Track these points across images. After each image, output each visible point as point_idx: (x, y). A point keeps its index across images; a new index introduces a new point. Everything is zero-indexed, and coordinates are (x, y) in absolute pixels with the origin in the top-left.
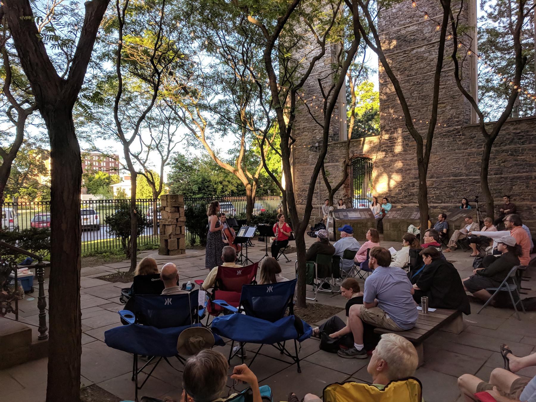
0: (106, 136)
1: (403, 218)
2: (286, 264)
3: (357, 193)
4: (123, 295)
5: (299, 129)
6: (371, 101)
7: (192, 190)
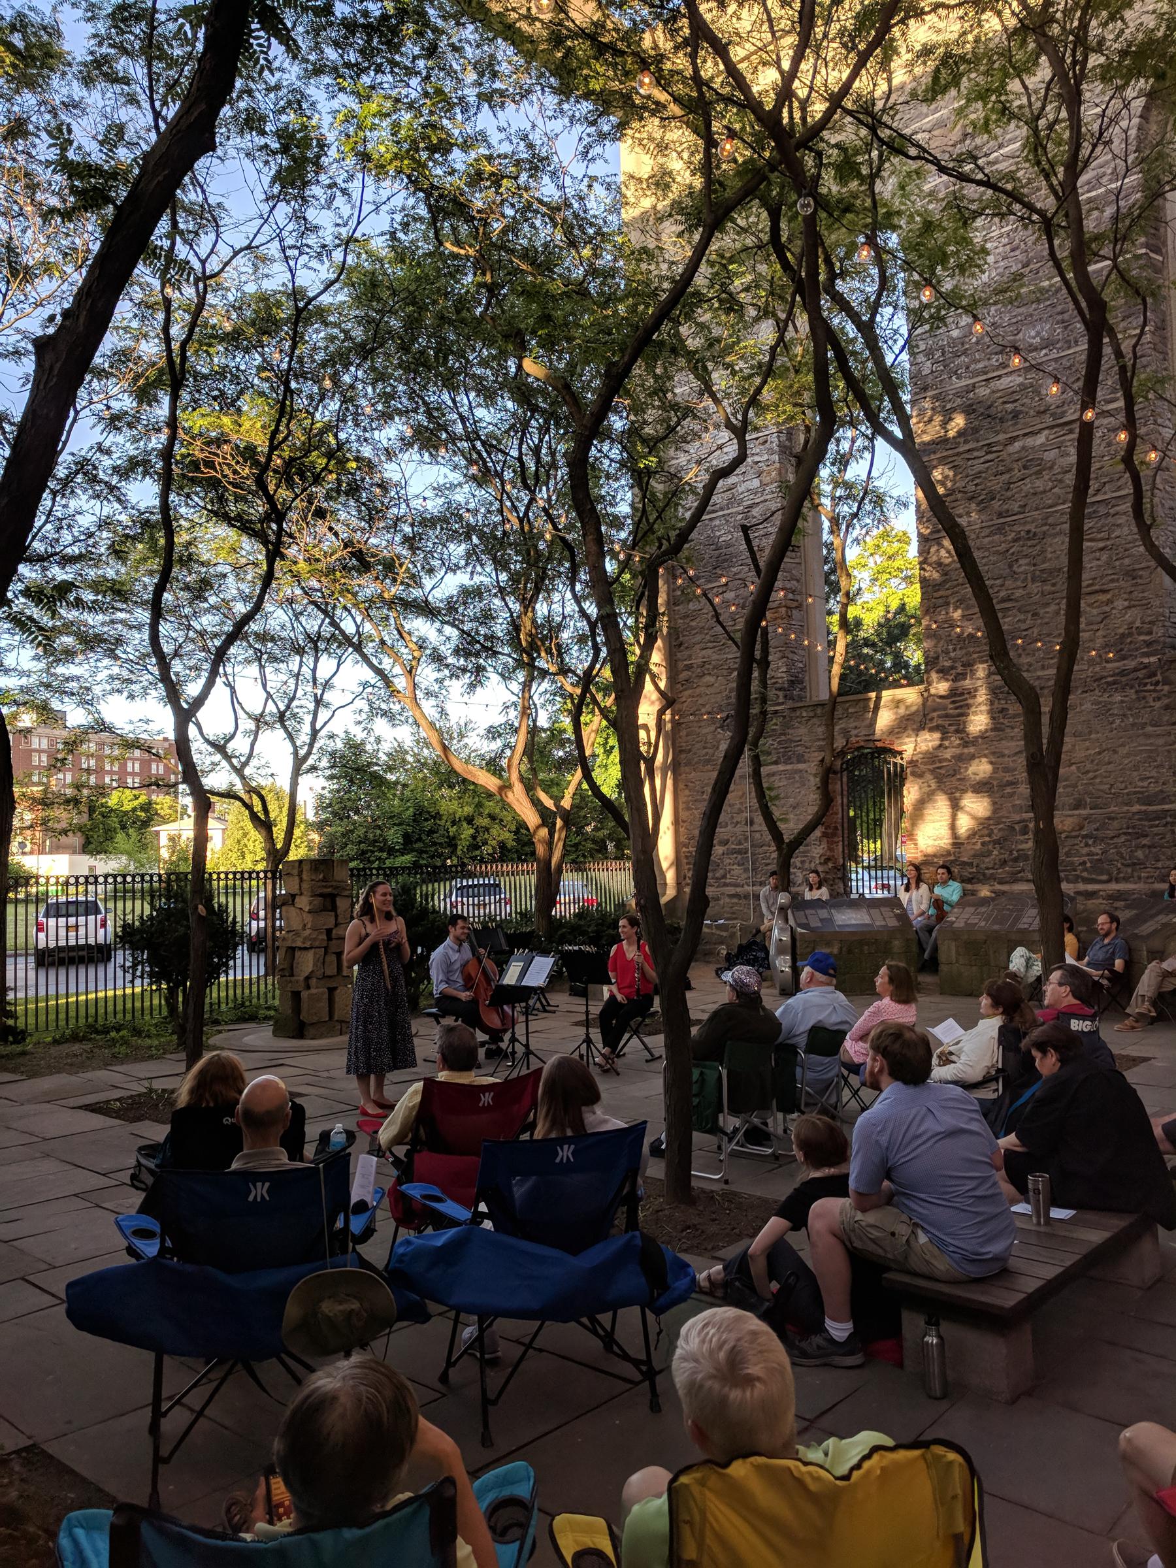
0: (136, 687)
1: (996, 927)
2: (646, 1066)
3: (869, 849)
4: (139, 1164)
5: (689, 667)
6: (903, 585)
7: (385, 840)
